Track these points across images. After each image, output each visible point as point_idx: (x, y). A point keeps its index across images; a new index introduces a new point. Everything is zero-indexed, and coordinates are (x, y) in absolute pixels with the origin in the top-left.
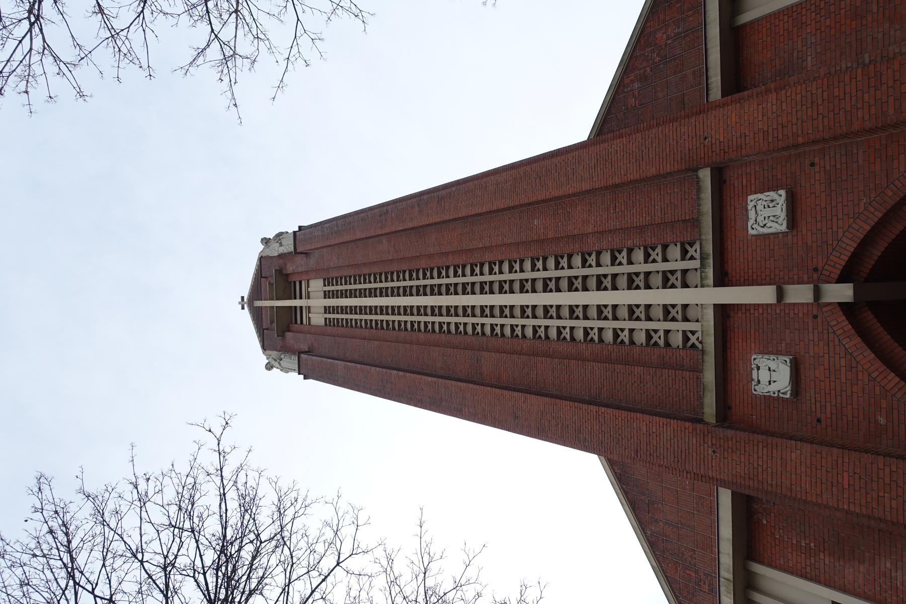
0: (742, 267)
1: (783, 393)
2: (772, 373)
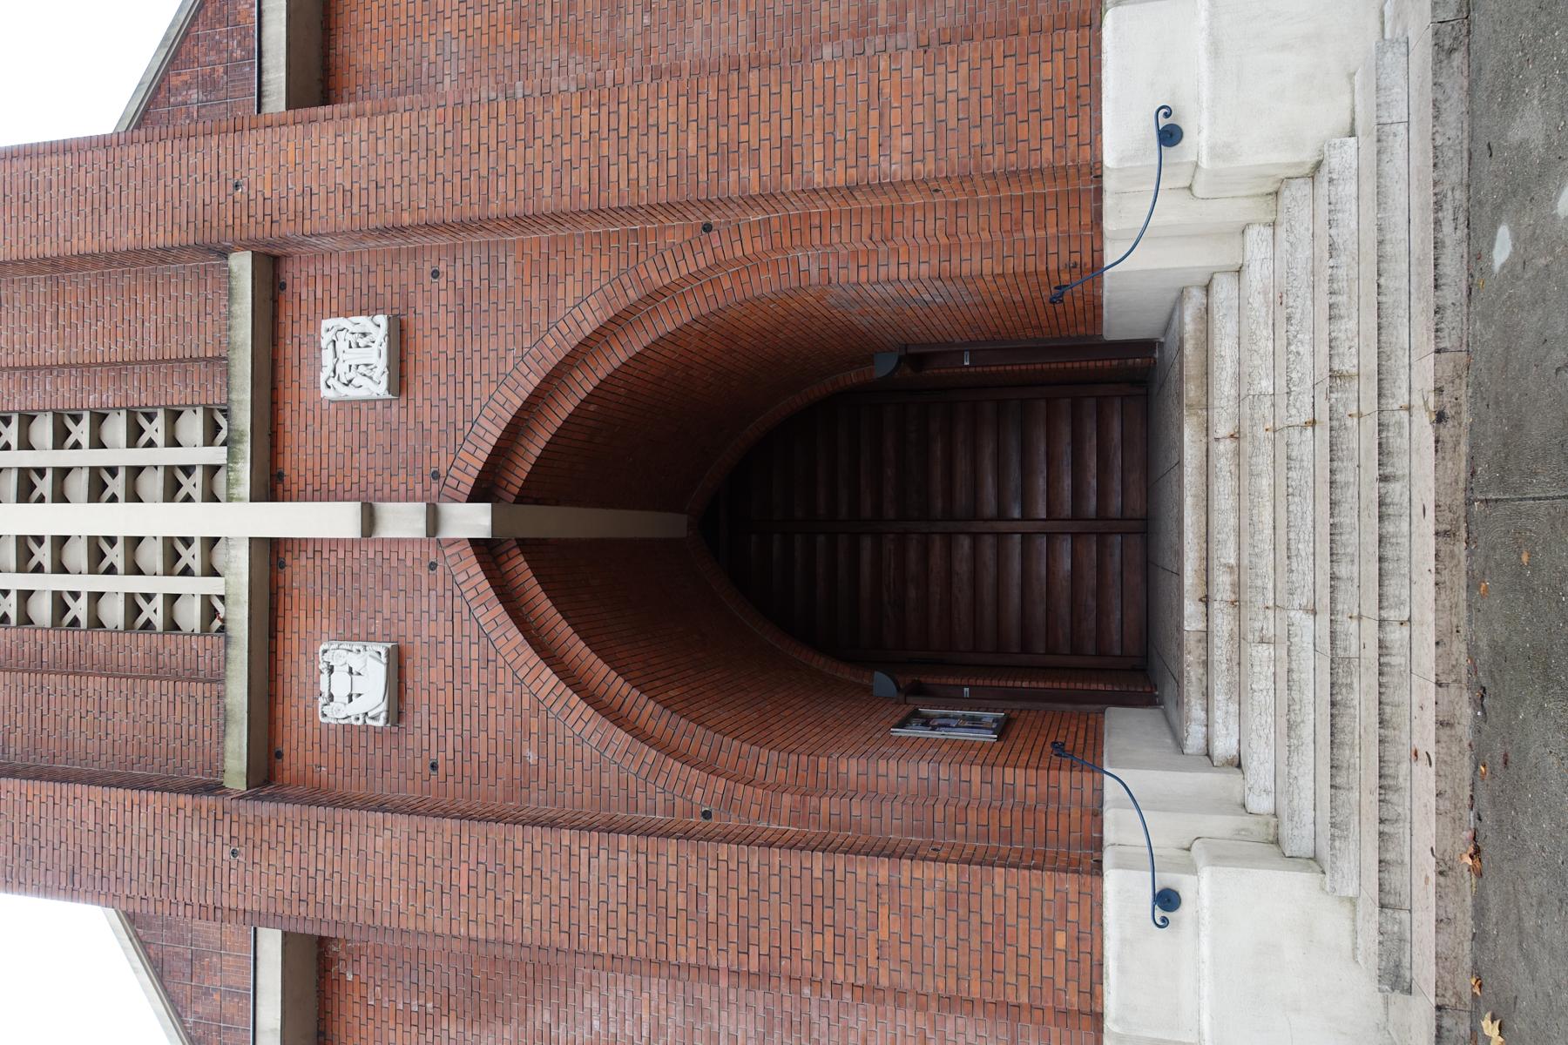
0: (310, 465)
1: (373, 718)
2: (355, 677)
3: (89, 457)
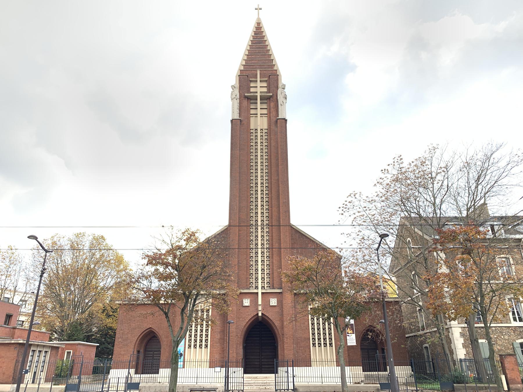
3: (264, 135)
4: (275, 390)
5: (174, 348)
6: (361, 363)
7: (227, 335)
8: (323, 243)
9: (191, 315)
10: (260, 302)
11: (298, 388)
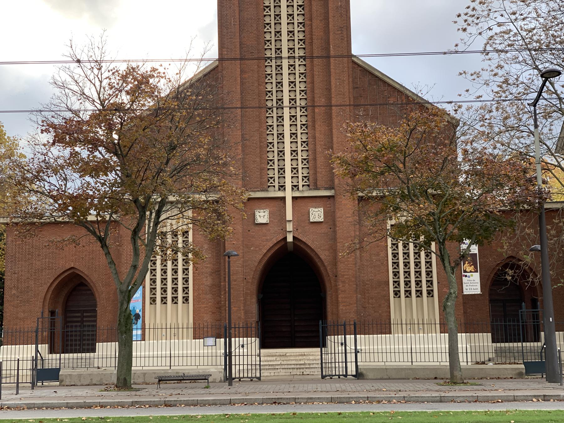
4: (320, 377)
5: (122, 304)
6: (490, 326)
7: (225, 278)
8: (420, 95)
9: (152, 242)
10: (289, 216)
11: (364, 372)
